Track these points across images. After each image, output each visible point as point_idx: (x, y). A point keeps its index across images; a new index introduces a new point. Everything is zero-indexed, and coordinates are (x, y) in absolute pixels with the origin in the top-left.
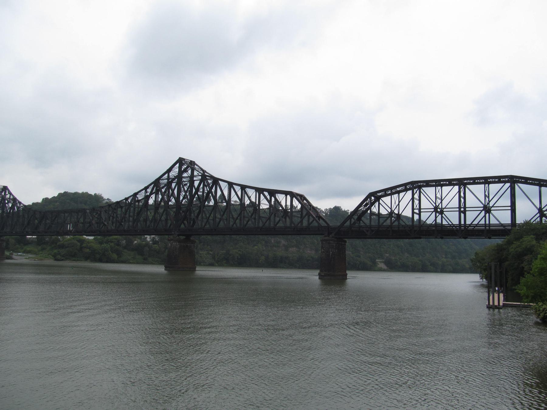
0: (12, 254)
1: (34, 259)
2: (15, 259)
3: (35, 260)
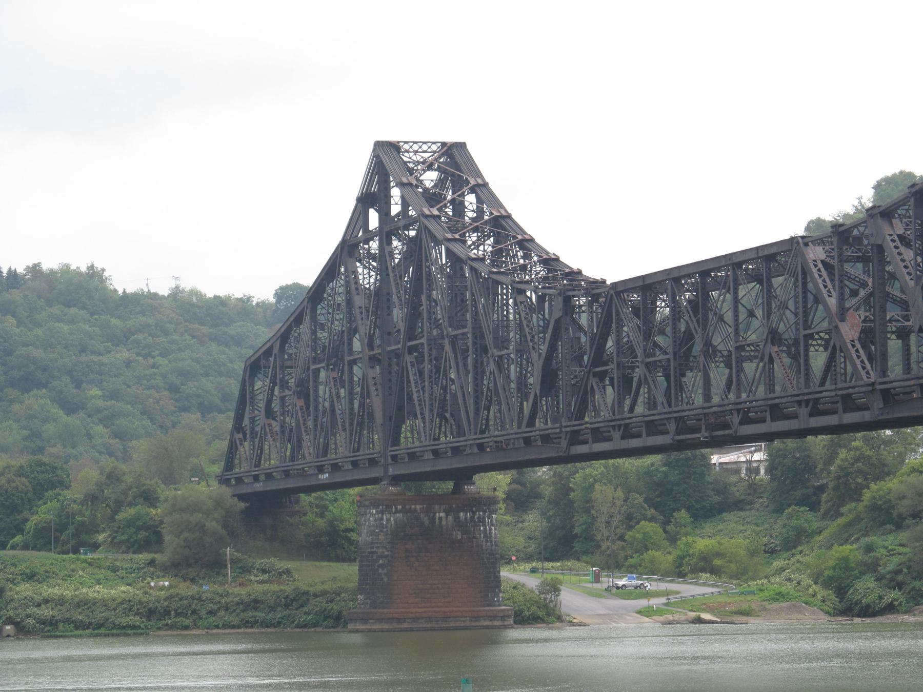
0: (554, 588)
1: (693, 615)
2: (571, 624)
3: (699, 621)
